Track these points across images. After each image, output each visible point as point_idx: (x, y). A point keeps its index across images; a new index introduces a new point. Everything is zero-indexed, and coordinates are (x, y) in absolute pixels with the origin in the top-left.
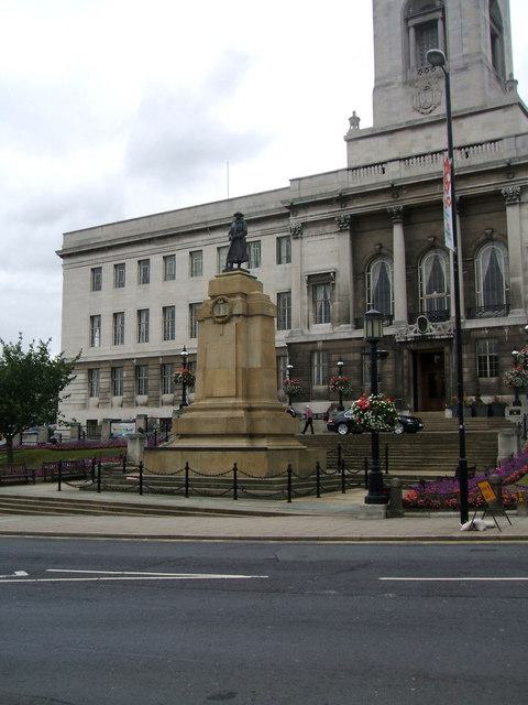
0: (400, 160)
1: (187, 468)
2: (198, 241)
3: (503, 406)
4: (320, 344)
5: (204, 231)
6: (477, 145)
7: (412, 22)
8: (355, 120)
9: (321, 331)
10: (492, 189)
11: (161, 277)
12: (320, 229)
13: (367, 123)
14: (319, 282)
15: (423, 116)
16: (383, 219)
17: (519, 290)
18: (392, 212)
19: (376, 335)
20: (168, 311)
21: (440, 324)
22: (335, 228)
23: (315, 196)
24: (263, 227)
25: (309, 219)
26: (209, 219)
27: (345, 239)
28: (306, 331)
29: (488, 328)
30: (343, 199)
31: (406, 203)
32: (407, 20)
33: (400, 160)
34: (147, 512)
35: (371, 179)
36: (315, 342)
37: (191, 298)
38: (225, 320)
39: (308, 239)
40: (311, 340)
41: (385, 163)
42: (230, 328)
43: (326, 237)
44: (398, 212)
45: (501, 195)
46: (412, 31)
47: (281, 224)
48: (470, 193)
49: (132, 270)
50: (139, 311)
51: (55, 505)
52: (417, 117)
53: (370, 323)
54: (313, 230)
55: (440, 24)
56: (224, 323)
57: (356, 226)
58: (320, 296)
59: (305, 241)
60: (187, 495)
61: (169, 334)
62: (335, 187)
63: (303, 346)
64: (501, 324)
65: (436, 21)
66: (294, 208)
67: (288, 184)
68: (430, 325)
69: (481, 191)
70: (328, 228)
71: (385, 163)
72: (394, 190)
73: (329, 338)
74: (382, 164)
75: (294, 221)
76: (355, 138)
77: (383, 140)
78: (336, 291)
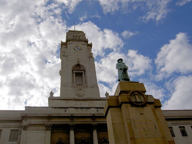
0: (74, 108)
7: (74, 71)
8: (52, 94)
13: (57, 94)
15: (79, 97)
16: (66, 128)
18: (71, 125)
22: (44, 128)
23: (92, 98)
24: (173, 122)
25: (32, 123)
27: (49, 133)
30: (50, 117)
32: (73, 71)
33: (74, 108)
35: (61, 112)
44: (50, 125)
46: (74, 74)
47: (14, 124)
52: (77, 97)
54: (33, 128)
55: (83, 74)
65: (82, 73)
69: (86, 123)
70: (40, 128)
72: (72, 117)
76: (51, 99)
77: (65, 102)
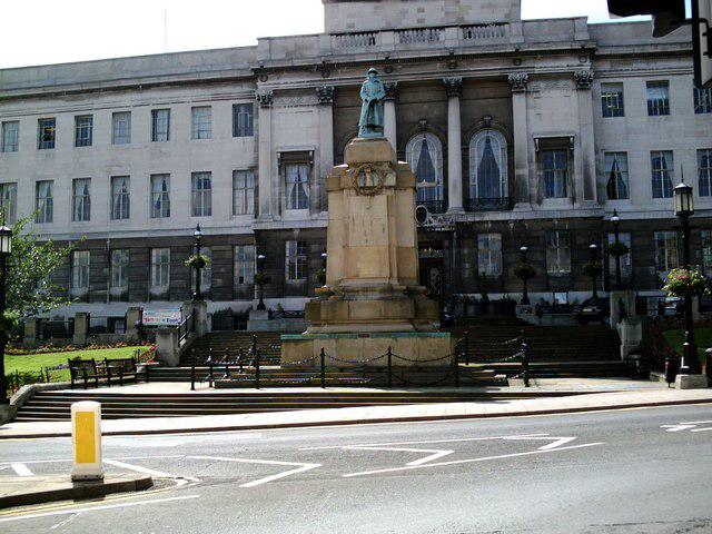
0: (395, 31)
1: (390, 354)
2: (126, 100)
3: (512, 303)
4: (296, 232)
5: (135, 88)
6: (481, 25)
9: (556, 206)
10: (497, 73)
11: (72, 140)
12: (295, 99)
14: (290, 159)
17: (524, 183)
19: (686, 208)
20: (202, 182)
21: (440, 217)
22: (314, 100)
25: (282, 87)
26: (142, 75)
27: (327, 113)
28: (277, 217)
29: (492, 222)
30: (325, 69)
31: (402, 79)
34: (403, 401)
36: (291, 230)
37: (39, 173)
38: (372, 192)
39: (280, 111)
40: (285, 227)
41: (377, 32)
42: (380, 201)
43: (303, 109)
45: (507, 80)
48: (473, 75)
49: (141, 122)
50: (38, 183)
51: (271, 401)
53: (679, 196)
54: (286, 100)
56: (372, 195)
57: (338, 100)
58: (292, 177)
59: (277, 111)
60: (457, 386)
61: (201, 208)
62: (313, 56)
63: (274, 234)
64: (507, 218)
66: (261, 73)
67: (256, 43)
68: (429, 216)
70: (305, 99)
71: (377, 32)
72: (451, 60)
73: (309, 226)
74: (372, 32)
75: (263, 88)
78: (315, 173)
